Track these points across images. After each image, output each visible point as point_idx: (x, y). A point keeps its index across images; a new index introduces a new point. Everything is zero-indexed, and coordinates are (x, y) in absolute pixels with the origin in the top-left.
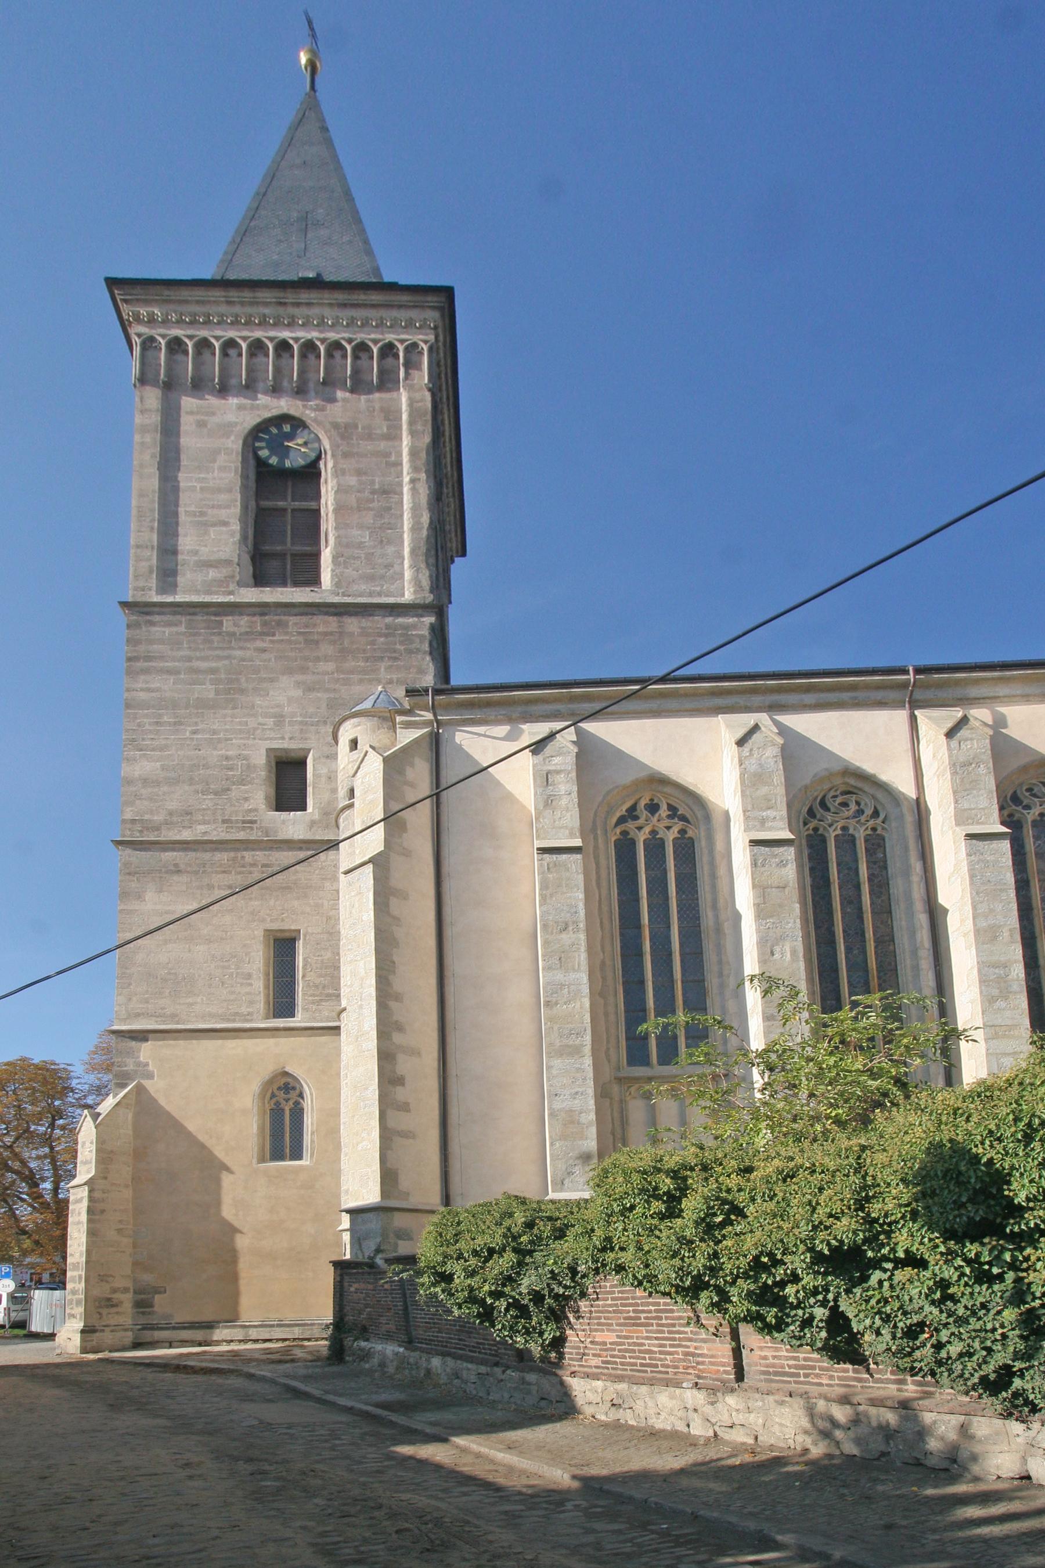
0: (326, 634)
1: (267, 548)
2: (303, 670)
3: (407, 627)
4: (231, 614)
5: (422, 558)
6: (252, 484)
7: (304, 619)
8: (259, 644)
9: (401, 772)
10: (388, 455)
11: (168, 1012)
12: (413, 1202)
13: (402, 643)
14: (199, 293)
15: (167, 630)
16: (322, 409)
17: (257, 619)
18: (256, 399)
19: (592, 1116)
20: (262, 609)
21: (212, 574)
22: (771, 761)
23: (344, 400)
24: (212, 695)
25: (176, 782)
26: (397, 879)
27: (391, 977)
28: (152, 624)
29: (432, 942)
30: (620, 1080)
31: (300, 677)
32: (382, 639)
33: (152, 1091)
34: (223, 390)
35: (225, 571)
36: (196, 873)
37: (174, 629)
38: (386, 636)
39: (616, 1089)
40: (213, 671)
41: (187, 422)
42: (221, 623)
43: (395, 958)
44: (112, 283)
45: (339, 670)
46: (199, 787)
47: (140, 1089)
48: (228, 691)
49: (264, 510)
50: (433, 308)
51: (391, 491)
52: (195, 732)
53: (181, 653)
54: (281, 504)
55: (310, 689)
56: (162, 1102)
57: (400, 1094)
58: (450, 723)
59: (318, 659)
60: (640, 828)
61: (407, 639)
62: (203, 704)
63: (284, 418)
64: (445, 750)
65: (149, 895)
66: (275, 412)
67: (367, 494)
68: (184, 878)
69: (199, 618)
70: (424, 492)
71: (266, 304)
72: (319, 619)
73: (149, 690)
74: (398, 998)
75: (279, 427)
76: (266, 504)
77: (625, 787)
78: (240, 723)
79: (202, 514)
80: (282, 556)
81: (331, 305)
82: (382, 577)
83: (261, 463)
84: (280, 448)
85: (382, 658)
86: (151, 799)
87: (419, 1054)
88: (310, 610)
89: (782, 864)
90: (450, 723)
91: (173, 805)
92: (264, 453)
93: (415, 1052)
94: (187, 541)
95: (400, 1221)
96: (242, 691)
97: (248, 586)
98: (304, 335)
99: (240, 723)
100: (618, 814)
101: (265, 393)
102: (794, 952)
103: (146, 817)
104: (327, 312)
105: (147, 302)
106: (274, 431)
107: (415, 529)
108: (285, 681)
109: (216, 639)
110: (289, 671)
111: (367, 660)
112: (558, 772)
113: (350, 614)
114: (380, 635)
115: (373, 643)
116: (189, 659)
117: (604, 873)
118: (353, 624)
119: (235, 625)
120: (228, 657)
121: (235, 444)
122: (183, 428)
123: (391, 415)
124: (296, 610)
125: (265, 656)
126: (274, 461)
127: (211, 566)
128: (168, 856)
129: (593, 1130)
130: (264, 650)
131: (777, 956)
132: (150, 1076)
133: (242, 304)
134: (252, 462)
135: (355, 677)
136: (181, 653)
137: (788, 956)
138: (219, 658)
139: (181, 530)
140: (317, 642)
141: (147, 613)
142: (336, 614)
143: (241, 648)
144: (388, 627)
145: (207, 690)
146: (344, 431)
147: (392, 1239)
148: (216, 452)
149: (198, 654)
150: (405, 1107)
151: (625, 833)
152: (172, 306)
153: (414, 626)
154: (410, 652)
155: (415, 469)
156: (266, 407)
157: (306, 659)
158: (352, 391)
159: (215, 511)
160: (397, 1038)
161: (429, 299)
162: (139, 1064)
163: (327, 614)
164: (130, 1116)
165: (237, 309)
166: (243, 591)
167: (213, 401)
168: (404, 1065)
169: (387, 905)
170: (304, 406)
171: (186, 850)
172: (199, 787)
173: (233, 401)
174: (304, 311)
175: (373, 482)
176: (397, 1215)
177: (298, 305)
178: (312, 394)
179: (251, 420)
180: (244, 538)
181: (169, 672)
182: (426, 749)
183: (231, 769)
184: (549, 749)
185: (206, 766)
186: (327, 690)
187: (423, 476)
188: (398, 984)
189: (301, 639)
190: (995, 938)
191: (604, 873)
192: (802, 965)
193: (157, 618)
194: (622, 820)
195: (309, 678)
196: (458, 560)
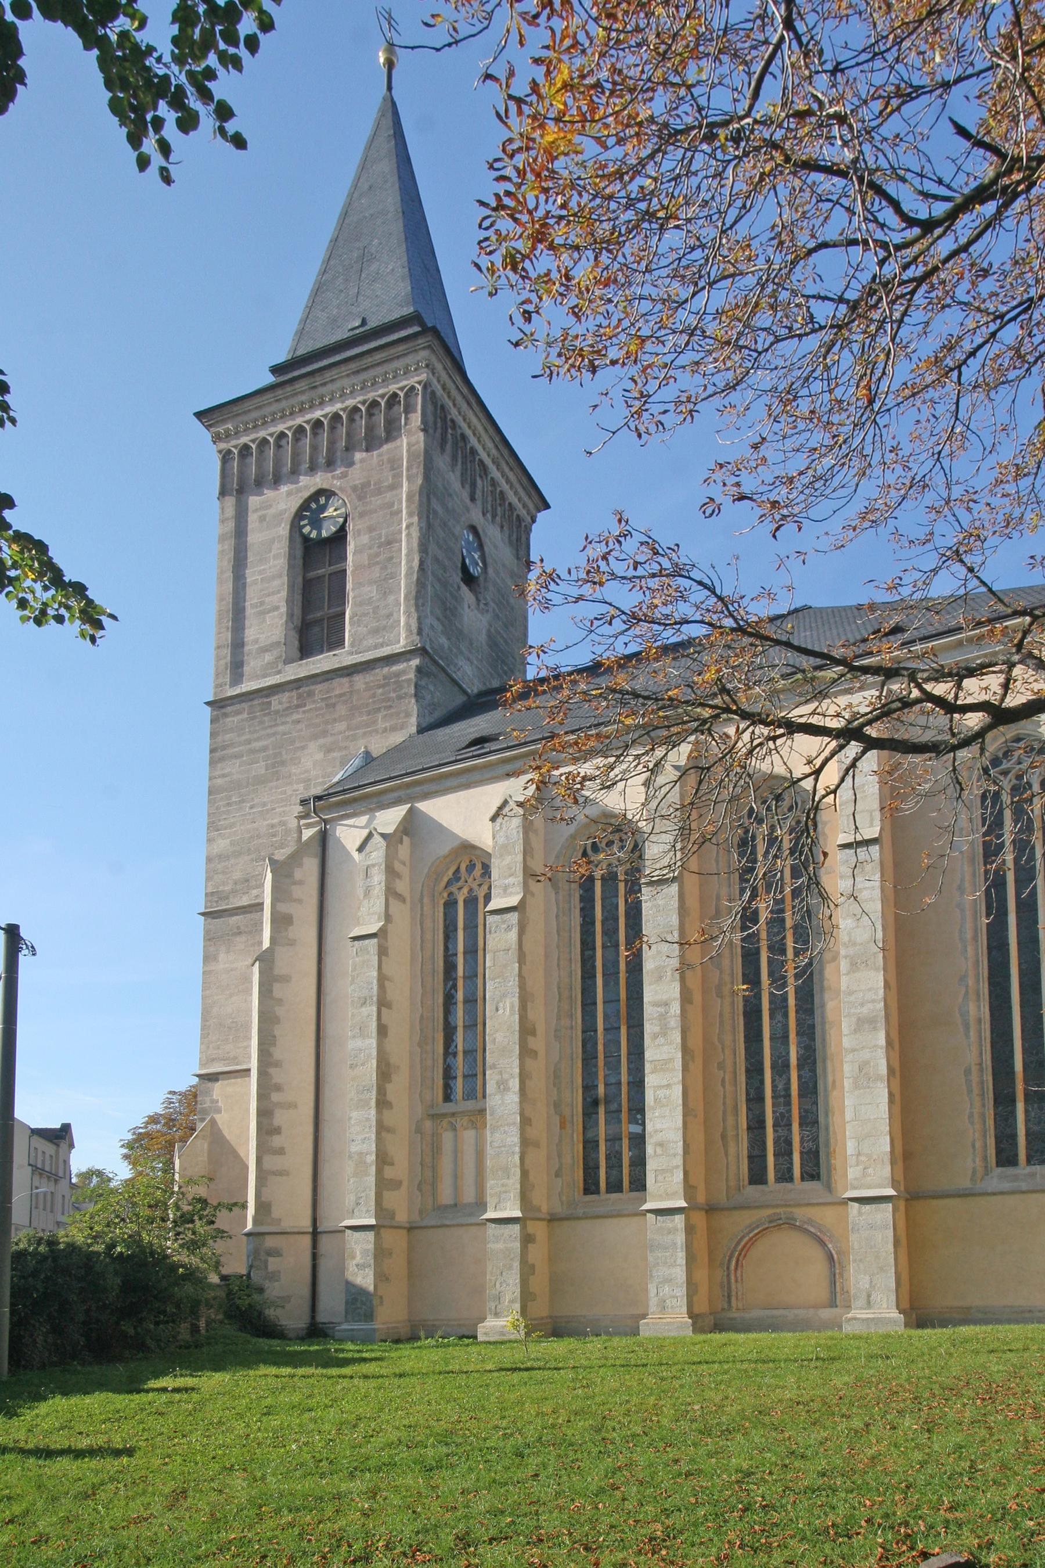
0: (341, 695)
1: (310, 617)
2: (324, 733)
3: (398, 674)
4: (277, 693)
5: (413, 602)
6: (300, 562)
7: (326, 685)
8: (295, 717)
9: (290, 875)
10: (392, 505)
11: (231, 1055)
12: (286, 1225)
13: (394, 691)
14: (257, 400)
15: (235, 719)
16: (344, 475)
17: (294, 693)
18: (297, 482)
19: (374, 1157)
20: (297, 683)
21: (268, 657)
22: (515, 832)
23: (362, 461)
24: (263, 772)
25: (237, 854)
26: (281, 967)
27: (272, 1049)
28: (226, 715)
29: (312, 1011)
30: (434, 1117)
31: (321, 741)
32: (380, 691)
33: (220, 1123)
34: (277, 481)
35: (276, 653)
36: (250, 932)
37: (240, 717)
38: (383, 686)
39: (428, 1124)
40: (265, 749)
41: (252, 518)
42: (270, 703)
43: (276, 1033)
44: (199, 415)
45: (349, 728)
46: (254, 856)
47: (213, 1122)
48: (273, 766)
49: (310, 580)
50: (424, 348)
51: (391, 541)
52: (251, 807)
53: (244, 738)
54: (321, 572)
55: (329, 750)
56: (226, 1132)
57: (277, 1141)
58: (333, 819)
59: (335, 720)
60: (460, 889)
61: (399, 685)
62: (260, 781)
63: (320, 492)
64: (331, 844)
65: (222, 956)
66: (313, 490)
67: (375, 549)
68: (243, 938)
69: (256, 702)
70: (415, 534)
71: (303, 392)
72: (336, 682)
73: (224, 776)
74: (277, 1064)
75: (317, 501)
76: (312, 574)
77: (445, 857)
78: (281, 793)
79: (262, 603)
80: (321, 620)
81: (348, 375)
82: (384, 628)
83: (306, 539)
84: (316, 523)
85: (379, 709)
86: (224, 873)
87: (296, 1107)
88: (329, 676)
89: (509, 928)
90: (333, 819)
91: (237, 875)
92: (306, 530)
93: (292, 1105)
94: (251, 633)
95: (270, 1242)
96: (283, 763)
97: (292, 661)
98: (329, 409)
99: (281, 793)
100: (446, 879)
101: (306, 475)
102: (512, 1006)
103: (221, 888)
104: (346, 382)
105: (224, 421)
106: (314, 506)
107: (408, 575)
108: (313, 746)
109: (266, 719)
110: (315, 737)
111: (369, 713)
112: (374, 865)
113: (358, 672)
114: (380, 687)
115: (374, 696)
116: (249, 742)
117: (428, 936)
118: (360, 681)
119: (280, 703)
120: (274, 734)
121: (283, 530)
122: (250, 527)
123: (394, 464)
124: (319, 679)
125: (299, 727)
126: (314, 535)
127: (267, 651)
128: (234, 920)
129: (374, 1168)
130: (298, 722)
131: (501, 1012)
132: (218, 1111)
133: (286, 398)
134: (299, 540)
135: (360, 731)
136: (244, 738)
137: (508, 1012)
138: (269, 736)
139: (247, 623)
140: (334, 705)
141: (223, 707)
142: (348, 675)
143: (283, 723)
144: (385, 678)
145: (259, 768)
146: (361, 492)
147: (263, 1256)
148: (272, 541)
149: (255, 736)
150: (281, 1151)
151: (450, 894)
152: (240, 419)
153: (404, 672)
154: (400, 698)
155: (410, 514)
156: (306, 487)
157: (327, 723)
158: (367, 450)
159: (270, 599)
160: (275, 1097)
161: (420, 341)
162: (213, 1101)
163: (341, 676)
164: (206, 1146)
165: (284, 404)
166: (288, 667)
167: (269, 493)
168: (280, 1118)
169: (271, 991)
170: (333, 477)
171: (244, 913)
172: (254, 856)
173: (284, 489)
174: (330, 387)
175: (380, 535)
176: (267, 1237)
177: (324, 384)
178: (339, 462)
179: (295, 503)
180: (290, 615)
181: (236, 756)
182: (316, 848)
183: (274, 836)
184: (368, 848)
185: (259, 837)
186: (340, 749)
187: (416, 519)
188: (277, 1053)
189: (323, 704)
190: (661, 977)
191: (428, 936)
192: (517, 1017)
193: (229, 709)
194: (449, 884)
195: (329, 739)
196: (541, 516)
